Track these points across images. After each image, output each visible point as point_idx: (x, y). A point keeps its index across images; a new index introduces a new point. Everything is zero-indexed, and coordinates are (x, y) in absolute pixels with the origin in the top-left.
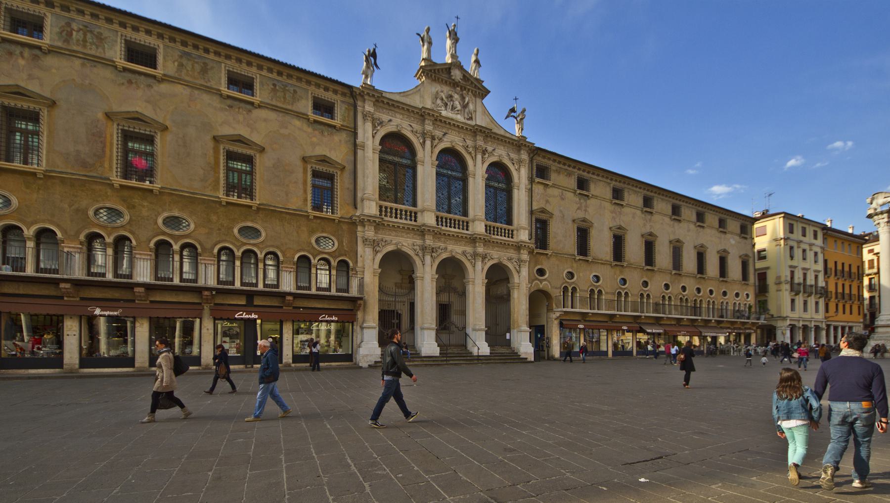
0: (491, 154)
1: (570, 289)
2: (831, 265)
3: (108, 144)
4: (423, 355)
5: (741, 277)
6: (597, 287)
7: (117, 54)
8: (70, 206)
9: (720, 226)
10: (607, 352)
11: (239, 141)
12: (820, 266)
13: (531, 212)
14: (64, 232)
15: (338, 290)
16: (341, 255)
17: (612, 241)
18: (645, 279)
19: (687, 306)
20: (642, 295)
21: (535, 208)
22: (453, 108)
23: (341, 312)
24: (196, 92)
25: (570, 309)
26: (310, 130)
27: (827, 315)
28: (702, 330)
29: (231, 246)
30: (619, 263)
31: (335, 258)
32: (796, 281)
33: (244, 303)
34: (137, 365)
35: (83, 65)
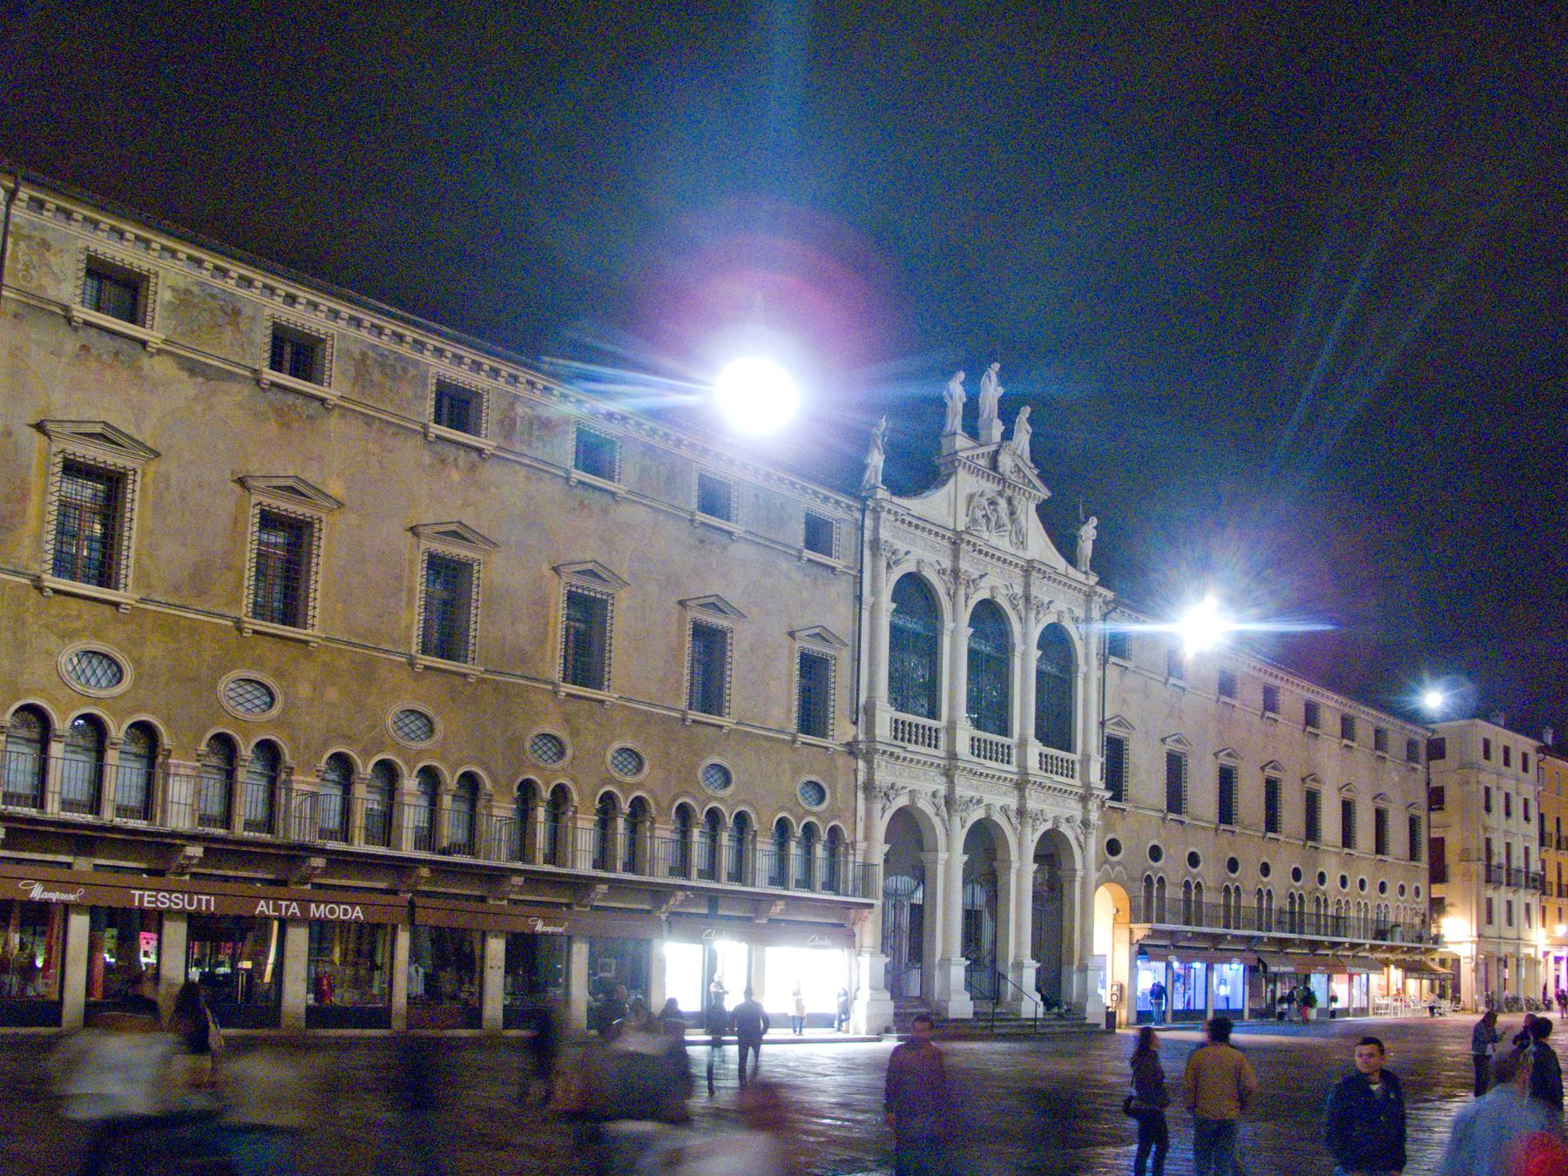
0: (1042, 607)
1: (1155, 880)
2: (1550, 827)
3: (552, 620)
4: (951, 1016)
5: (1303, 830)
6: (1265, 885)
7: (68, 288)
8: (503, 733)
9: (1377, 748)
10: (1242, 1011)
11: (455, 534)
12: (1533, 829)
13: (1102, 724)
14: (495, 781)
15: (67, 805)
16: (832, 818)
17: (1373, 816)
18: (1265, 860)
19: (1365, 919)
20: (1187, 885)
21: (1107, 716)
22: (999, 526)
23: (373, 897)
24: (661, 517)
25: (541, 866)
26: (798, 577)
27: (1490, 931)
28: (1266, 960)
29: (38, 702)
30: (1228, 827)
31: (119, 715)
32: (1514, 865)
33: (705, 911)
34: (65, 1024)
35: (527, 478)
